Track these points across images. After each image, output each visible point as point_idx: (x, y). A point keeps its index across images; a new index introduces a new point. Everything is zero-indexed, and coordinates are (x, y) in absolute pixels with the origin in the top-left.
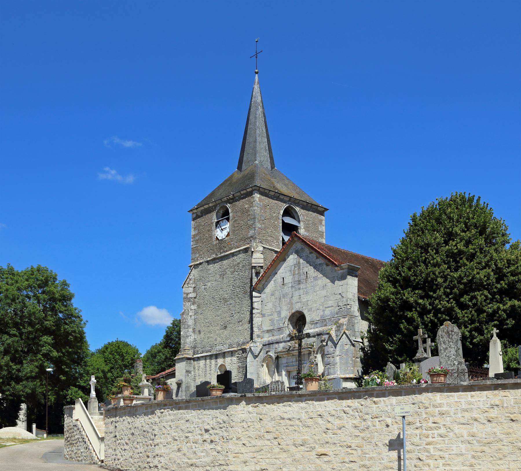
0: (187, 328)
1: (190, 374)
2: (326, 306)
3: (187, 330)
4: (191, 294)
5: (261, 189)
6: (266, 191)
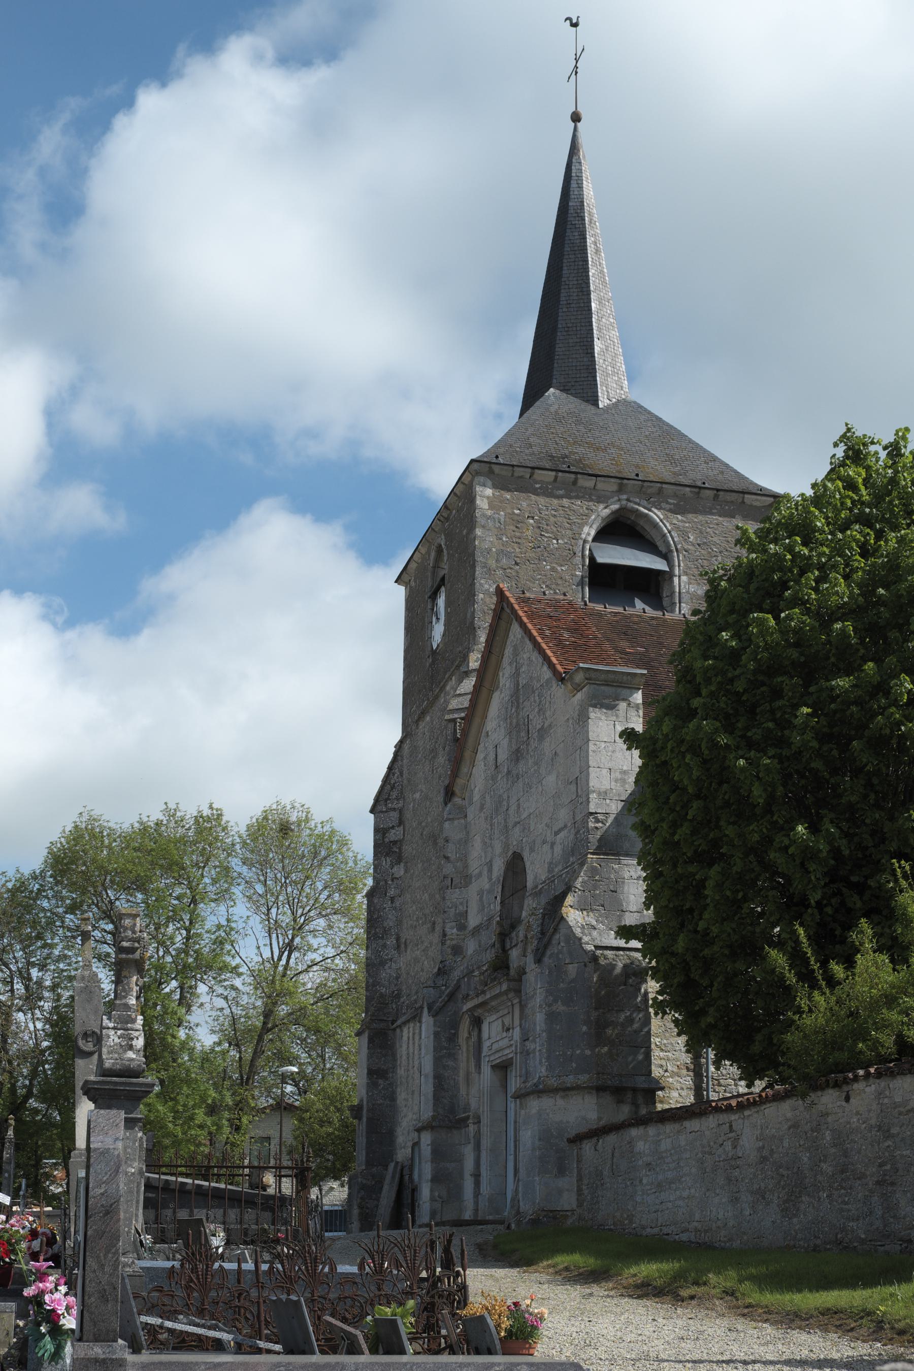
0: (382, 938)
1: (380, 1081)
2: (555, 828)
3: (381, 942)
4: (393, 831)
5: (496, 469)
6: (519, 472)
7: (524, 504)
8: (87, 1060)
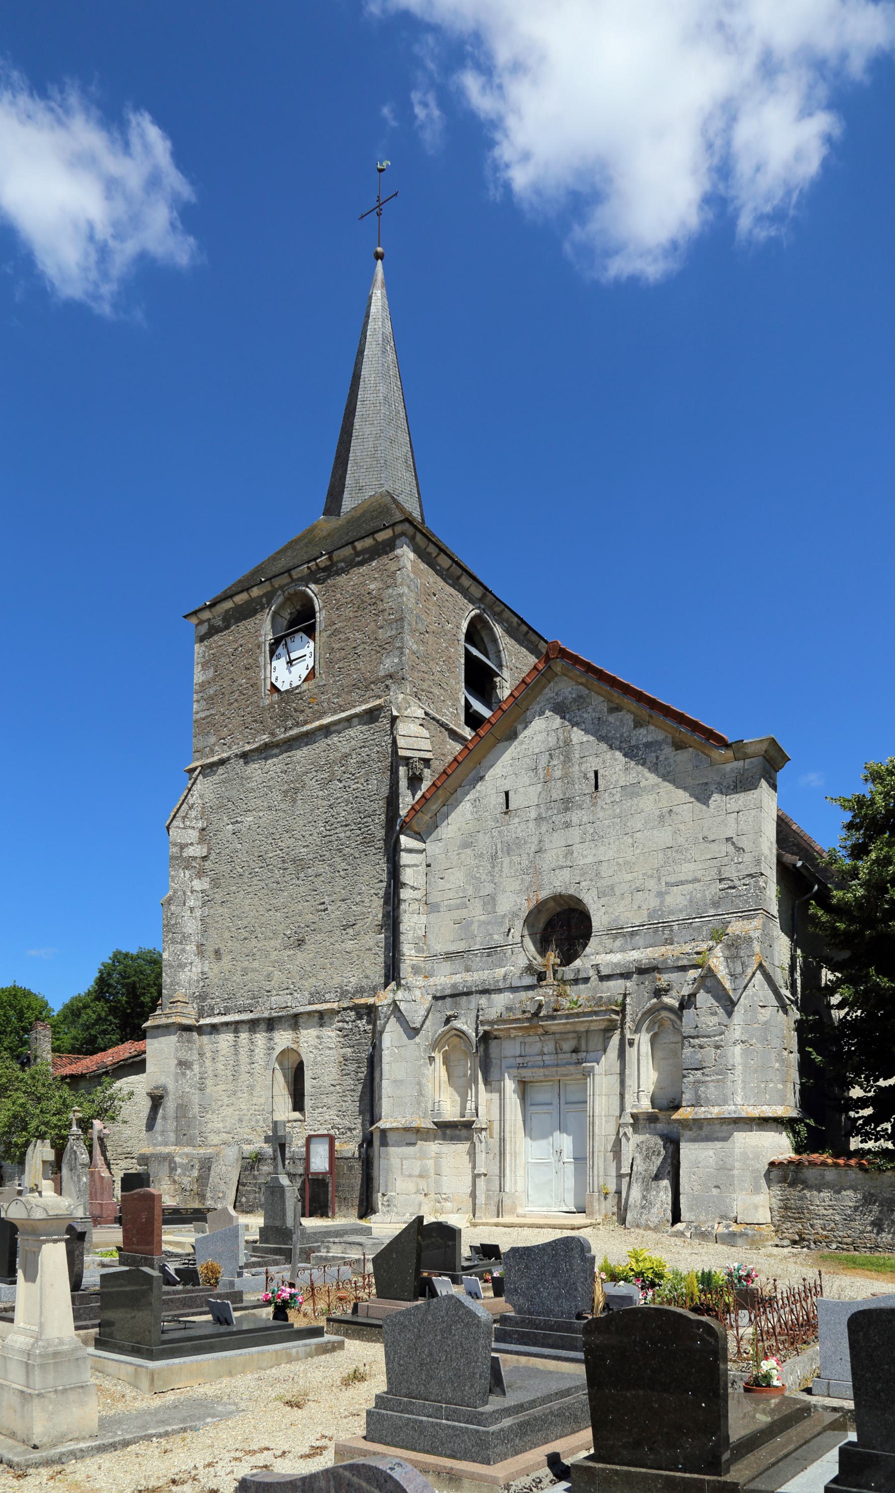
0: (181, 943)
1: (188, 1072)
3: (179, 947)
8: (544, 895)
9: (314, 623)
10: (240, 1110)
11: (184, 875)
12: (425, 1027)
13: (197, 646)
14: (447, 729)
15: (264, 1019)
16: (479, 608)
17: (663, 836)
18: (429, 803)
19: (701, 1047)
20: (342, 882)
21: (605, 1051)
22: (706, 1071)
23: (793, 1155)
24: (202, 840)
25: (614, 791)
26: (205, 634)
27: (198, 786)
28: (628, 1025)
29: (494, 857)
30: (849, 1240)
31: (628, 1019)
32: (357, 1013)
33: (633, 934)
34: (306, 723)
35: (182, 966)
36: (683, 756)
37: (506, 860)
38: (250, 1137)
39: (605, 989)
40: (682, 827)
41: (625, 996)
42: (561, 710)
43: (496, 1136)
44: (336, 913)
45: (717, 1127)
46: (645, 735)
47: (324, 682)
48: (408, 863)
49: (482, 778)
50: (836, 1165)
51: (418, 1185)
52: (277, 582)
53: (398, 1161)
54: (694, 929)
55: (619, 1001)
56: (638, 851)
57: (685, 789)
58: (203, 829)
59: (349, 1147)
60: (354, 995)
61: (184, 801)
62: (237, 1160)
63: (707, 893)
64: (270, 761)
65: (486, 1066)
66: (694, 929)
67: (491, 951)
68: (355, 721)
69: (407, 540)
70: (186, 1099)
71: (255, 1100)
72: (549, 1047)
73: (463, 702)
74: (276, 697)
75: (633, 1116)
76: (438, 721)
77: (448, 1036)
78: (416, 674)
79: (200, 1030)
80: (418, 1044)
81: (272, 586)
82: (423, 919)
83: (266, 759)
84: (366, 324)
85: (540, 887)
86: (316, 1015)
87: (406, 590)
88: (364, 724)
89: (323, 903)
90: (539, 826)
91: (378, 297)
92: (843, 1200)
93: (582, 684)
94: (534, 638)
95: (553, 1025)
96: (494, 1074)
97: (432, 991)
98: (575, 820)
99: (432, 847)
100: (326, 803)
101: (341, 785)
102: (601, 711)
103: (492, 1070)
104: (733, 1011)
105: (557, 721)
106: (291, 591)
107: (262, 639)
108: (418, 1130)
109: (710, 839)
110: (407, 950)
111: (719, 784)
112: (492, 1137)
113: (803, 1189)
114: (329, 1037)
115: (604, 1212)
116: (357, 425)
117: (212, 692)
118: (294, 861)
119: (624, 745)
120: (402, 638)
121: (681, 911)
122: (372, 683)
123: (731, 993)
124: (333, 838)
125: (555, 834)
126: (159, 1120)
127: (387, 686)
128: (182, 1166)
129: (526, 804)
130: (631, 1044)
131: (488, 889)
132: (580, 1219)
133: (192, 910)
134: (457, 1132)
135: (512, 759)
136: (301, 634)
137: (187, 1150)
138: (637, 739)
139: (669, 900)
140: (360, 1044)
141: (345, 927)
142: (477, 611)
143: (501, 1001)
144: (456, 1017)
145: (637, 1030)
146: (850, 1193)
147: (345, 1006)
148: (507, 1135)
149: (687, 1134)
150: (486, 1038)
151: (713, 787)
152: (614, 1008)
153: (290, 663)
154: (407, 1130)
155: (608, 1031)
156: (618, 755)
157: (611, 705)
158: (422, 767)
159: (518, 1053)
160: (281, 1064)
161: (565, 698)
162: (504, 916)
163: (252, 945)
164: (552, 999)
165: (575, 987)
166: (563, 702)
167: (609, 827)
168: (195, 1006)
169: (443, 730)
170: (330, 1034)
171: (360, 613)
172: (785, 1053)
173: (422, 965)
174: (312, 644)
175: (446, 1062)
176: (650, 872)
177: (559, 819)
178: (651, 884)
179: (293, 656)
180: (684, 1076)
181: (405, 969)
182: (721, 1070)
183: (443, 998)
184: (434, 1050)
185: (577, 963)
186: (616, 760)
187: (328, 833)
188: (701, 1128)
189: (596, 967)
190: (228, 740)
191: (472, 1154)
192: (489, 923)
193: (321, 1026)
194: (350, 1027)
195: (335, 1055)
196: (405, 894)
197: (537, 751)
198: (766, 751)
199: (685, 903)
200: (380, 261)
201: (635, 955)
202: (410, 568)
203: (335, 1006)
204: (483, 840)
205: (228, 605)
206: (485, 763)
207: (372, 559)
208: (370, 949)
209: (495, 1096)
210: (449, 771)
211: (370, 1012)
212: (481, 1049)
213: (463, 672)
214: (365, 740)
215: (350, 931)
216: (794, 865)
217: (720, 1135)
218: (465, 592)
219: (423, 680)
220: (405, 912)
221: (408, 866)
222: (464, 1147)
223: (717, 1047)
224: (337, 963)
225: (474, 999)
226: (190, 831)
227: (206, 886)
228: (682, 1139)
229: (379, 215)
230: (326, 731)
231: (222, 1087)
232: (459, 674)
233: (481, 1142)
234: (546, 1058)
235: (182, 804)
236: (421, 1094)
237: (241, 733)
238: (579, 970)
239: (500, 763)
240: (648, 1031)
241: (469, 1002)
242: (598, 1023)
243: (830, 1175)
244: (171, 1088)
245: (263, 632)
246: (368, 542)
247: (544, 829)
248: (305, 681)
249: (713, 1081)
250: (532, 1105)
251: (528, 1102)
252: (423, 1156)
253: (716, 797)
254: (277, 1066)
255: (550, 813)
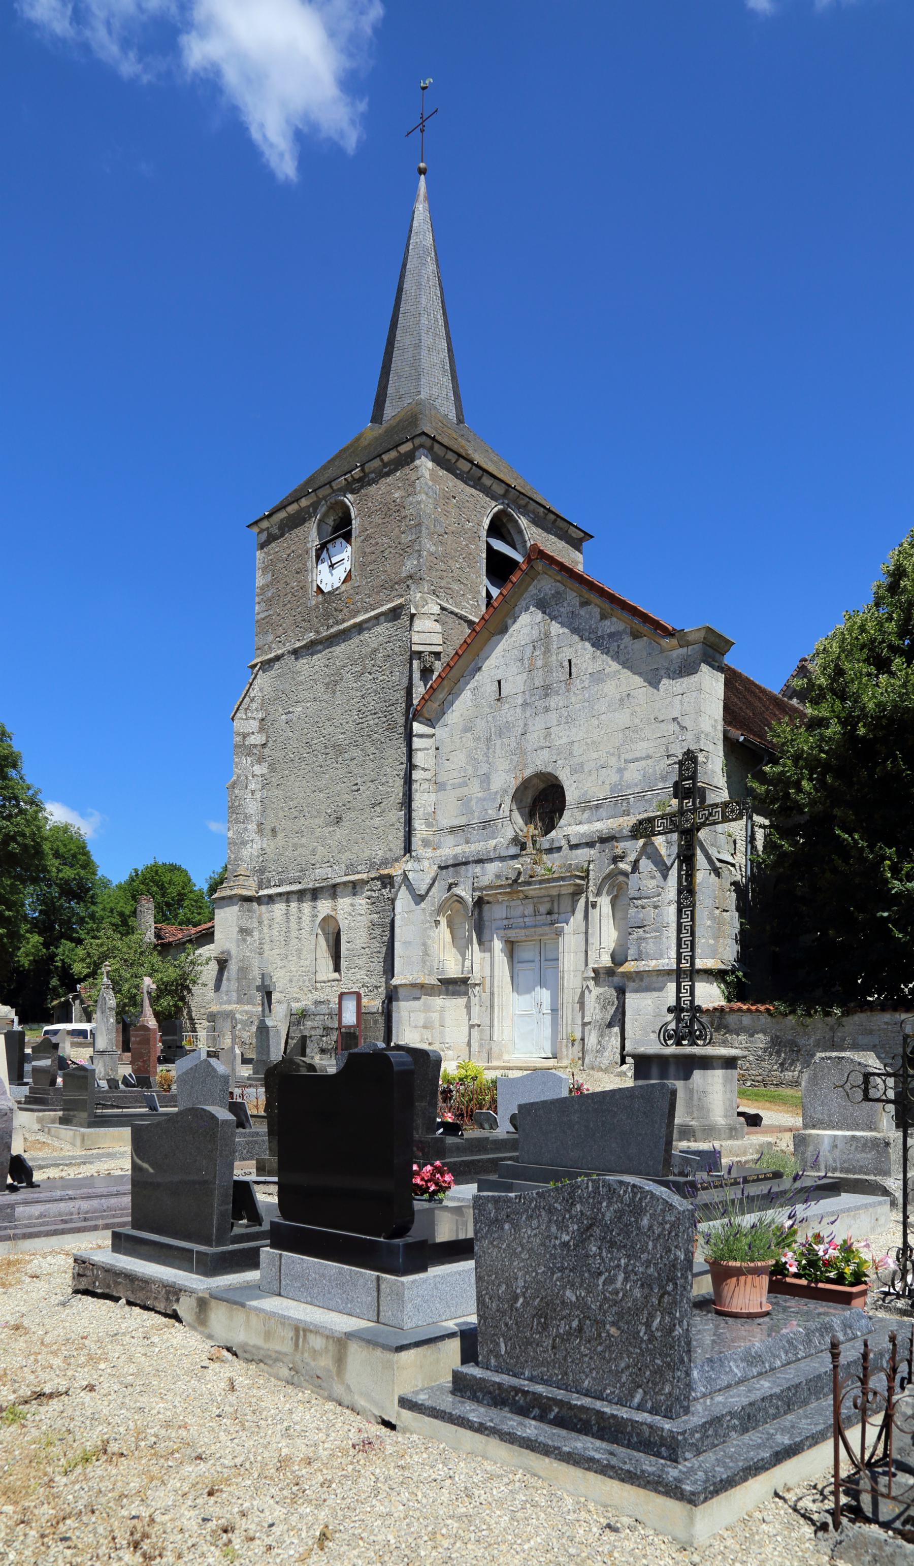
0: (243, 823)
1: (248, 938)
3: (242, 826)
7: (451, 484)
8: (528, 773)
9: (351, 530)
10: (291, 971)
11: (247, 761)
12: (431, 894)
13: (258, 553)
14: (466, 621)
15: (309, 889)
16: (502, 503)
17: (622, 718)
18: (437, 693)
19: (643, 907)
20: (372, 765)
21: (573, 912)
22: (647, 928)
23: (723, 1003)
24: (261, 730)
25: (584, 678)
26: (265, 541)
27: (258, 681)
28: (591, 888)
29: (489, 740)
30: (759, 1078)
31: (591, 883)
32: (383, 883)
33: (597, 807)
34: (344, 621)
35: (244, 843)
36: (640, 645)
37: (499, 742)
38: (298, 996)
39: (574, 857)
40: (637, 709)
41: (589, 862)
42: (542, 605)
43: (488, 990)
44: (367, 792)
45: (654, 978)
46: (611, 626)
47: (358, 584)
48: (419, 747)
49: (480, 669)
50: (757, 1011)
51: (422, 1035)
52: (321, 493)
53: (406, 1014)
54: (646, 801)
55: (585, 868)
56: (603, 732)
57: (640, 674)
58: (263, 720)
59: (374, 1003)
60: (380, 866)
61: (246, 695)
62: (286, 1016)
63: (657, 768)
64: (315, 657)
65: (480, 928)
66: (646, 801)
67: (486, 824)
68: (382, 618)
69: (426, 451)
70: (246, 962)
71: (302, 963)
72: (529, 910)
73: (484, 594)
74: (320, 597)
75: (594, 970)
76: (456, 615)
77: (450, 902)
78: (434, 573)
79: (259, 900)
80: (424, 909)
81: (317, 496)
82: (433, 796)
83: (312, 654)
84: (409, 238)
85: (525, 766)
86: (351, 885)
87: (424, 497)
88: (389, 622)
89: (357, 784)
90: (524, 711)
91: (421, 210)
92: (755, 1042)
93: (559, 581)
94: (560, 523)
95: (531, 890)
96: (486, 937)
97: (438, 862)
98: (553, 705)
99: (440, 732)
100: (359, 693)
101: (371, 677)
102: (574, 606)
103: (485, 931)
104: (667, 875)
105: (539, 616)
106: (333, 501)
107: (309, 545)
108: (422, 986)
109: (660, 719)
110: (419, 825)
111: (668, 669)
112: (484, 992)
113: (725, 1033)
114: (360, 905)
115: (571, 1057)
116: (398, 338)
117: (270, 595)
118: (334, 746)
119: (592, 636)
120: (420, 542)
121: (636, 785)
122: (396, 583)
123: (665, 859)
124: (365, 725)
125: (537, 718)
126: (224, 982)
127: (408, 586)
128: (241, 1021)
129: (514, 691)
130: (594, 906)
131: (484, 768)
132: (551, 1063)
133: (253, 792)
134: (457, 988)
135: (504, 651)
136: (341, 540)
137: (247, 1008)
138: (603, 630)
139: (627, 775)
140: (384, 911)
141: (374, 806)
142: (501, 507)
143: (492, 868)
144: (456, 884)
145: (598, 894)
146: (761, 1036)
147: (373, 876)
148: (496, 990)
149: (631, 985)
150: (480, 903)
151: (662, 672)
152: (578, 873)
153: (332, 566)
154: (413, 985)
155: (578, 892)
156: (587, 645)
157: (582, 599)
158: (433, 659)
159: (504, 916)
160: (323, 930)
161: (546, 594)
162: (496, 793)
163: (301, 824)
164: (529, 867)
165: (550, 856)
166: (544, 597)
167: (580, 710)
168: (256, 879)
169: (462, 622)
170: (361, 902)
171: (387, 520)
172: (717, 912)
173: (431, 838)
174: (349, 548)
175: (450, 925)
176: (612, 751)
177: (540, 704)
178: (613, 761)
179: (334, 560)
180: (630, 934)
181: (416, 842)
182: (658, 927)
183: (446, 867)
184: (438, 914)
185: (553, 834)
186: (585, 649)
187: (361, 721)
188: (642, 980)
189: (567, 837)
190: (283, 638)
191: (468, 1007)
192: (485, 799)
193: (354, 895)
194: (377, 895)
195: (364, 921)
196: (416, 775)
197: (523, 643)
198: (704, 638)
199: (640, 778)
200: (423, 176)
201: (598, 826)
202: (428, 477)
203: (364, 876)
204: (480, 724)
205: (282, 515)
206: (482, 655)
207: (396, 470)
208: (393, 825)
209: (487, 955)
210: (452, 664)
211: (387, 881)
212: (476, 913)
213: (485, 565)
214: (390, 636)
215: (377, 809)
216: (738, 740)
217: (656, 985)
218: (487, 491)
219: (441, 578)
220: (417, 791)
221: (420, 750)
222: (462, 1001)
223: (656, 907)
224: (367, 838)
225: (470, 867)
226: (251, 722)
227: (265, 771)
228: (627, 990)
229: (422, 131)
230: (360, 628)
231: (276, 951)
232: (480, 568)
233: (475, 996)
234: (526, 919)
235: (244, 697)
236: (426, 953)
237: (293, 631)
238: (553, 840)
239: (494, 655)
240: (608, 893)
241: (467, 871)
242: (566, 888)
243: (746, 1020)
244: (234, 952)
245: (310, 539)
246: (393, 454)
247: (528, 713)
248: (344, 582)
249: (651, 937)
250: (519, 962)
251: (516, 960)
252: (427, 1009)
253: (665, 681)
254: (320, 932)
255: (533, 699)
